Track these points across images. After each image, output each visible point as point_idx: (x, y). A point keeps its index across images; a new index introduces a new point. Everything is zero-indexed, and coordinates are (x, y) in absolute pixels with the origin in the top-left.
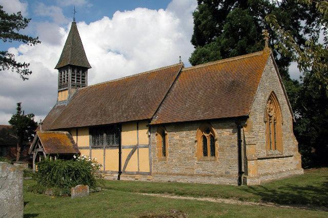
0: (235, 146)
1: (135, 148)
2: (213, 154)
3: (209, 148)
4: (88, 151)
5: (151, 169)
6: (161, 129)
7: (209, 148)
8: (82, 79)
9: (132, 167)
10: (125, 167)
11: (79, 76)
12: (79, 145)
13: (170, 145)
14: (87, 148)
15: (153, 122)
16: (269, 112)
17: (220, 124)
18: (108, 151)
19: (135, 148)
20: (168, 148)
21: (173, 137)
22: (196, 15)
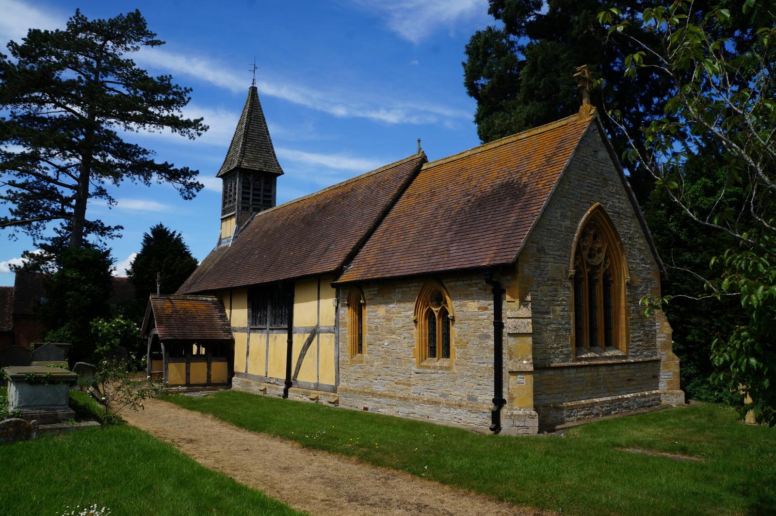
0: (488, 337)
1: (314, 332)
2: (447, 354)
3: (437, 341)
4: (245, 335)
5: (337, 380)
6: (356, 295)
7: (437, 341)
8: (265, 196)
9: (305, 376)
10: (296, 374)
11: (259, 190)
12: (233, 324)
13: (370, 330)
14: (242, 330)
15: (343, 279)
16: (590, 256)
17: (613, 304)
18: (273, 335)
19: (314, 332)
20: (366, 336)
21: (376, 314)
22: (138, 255)
